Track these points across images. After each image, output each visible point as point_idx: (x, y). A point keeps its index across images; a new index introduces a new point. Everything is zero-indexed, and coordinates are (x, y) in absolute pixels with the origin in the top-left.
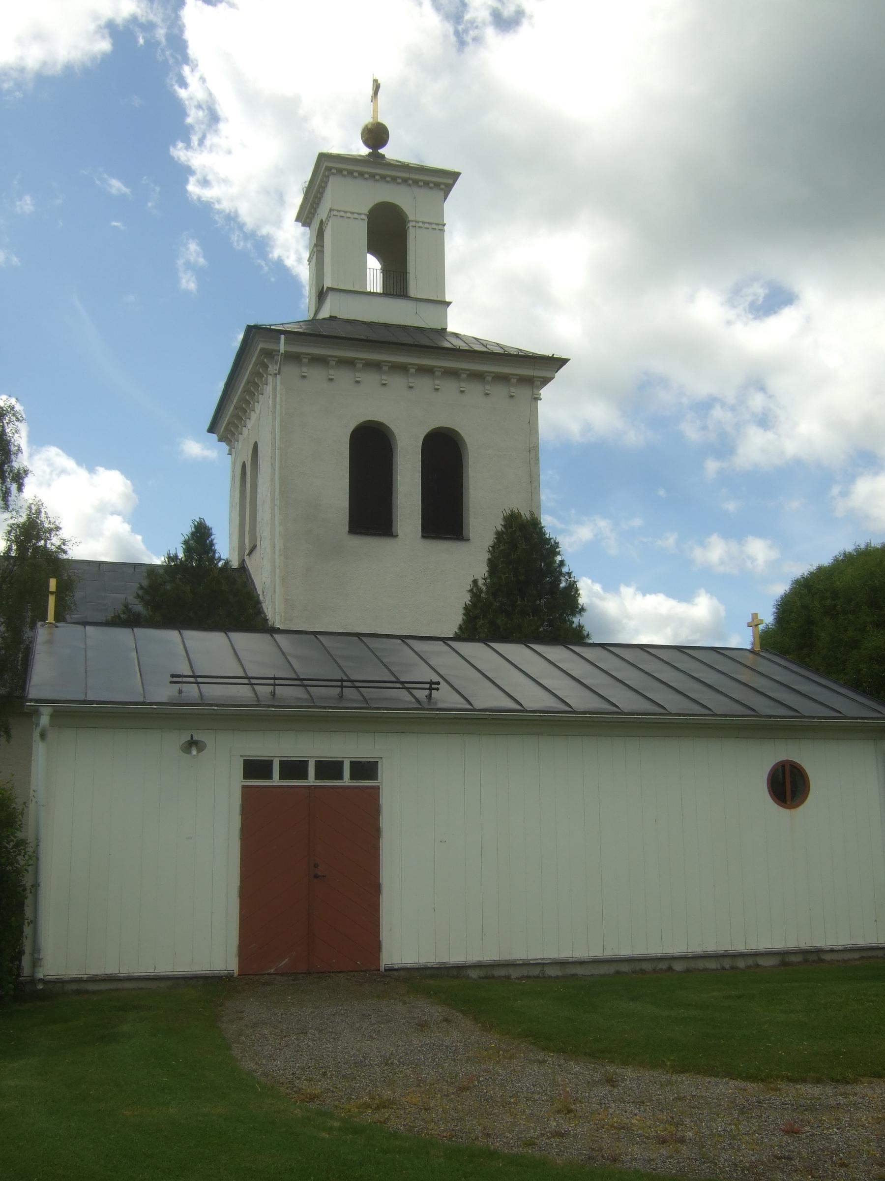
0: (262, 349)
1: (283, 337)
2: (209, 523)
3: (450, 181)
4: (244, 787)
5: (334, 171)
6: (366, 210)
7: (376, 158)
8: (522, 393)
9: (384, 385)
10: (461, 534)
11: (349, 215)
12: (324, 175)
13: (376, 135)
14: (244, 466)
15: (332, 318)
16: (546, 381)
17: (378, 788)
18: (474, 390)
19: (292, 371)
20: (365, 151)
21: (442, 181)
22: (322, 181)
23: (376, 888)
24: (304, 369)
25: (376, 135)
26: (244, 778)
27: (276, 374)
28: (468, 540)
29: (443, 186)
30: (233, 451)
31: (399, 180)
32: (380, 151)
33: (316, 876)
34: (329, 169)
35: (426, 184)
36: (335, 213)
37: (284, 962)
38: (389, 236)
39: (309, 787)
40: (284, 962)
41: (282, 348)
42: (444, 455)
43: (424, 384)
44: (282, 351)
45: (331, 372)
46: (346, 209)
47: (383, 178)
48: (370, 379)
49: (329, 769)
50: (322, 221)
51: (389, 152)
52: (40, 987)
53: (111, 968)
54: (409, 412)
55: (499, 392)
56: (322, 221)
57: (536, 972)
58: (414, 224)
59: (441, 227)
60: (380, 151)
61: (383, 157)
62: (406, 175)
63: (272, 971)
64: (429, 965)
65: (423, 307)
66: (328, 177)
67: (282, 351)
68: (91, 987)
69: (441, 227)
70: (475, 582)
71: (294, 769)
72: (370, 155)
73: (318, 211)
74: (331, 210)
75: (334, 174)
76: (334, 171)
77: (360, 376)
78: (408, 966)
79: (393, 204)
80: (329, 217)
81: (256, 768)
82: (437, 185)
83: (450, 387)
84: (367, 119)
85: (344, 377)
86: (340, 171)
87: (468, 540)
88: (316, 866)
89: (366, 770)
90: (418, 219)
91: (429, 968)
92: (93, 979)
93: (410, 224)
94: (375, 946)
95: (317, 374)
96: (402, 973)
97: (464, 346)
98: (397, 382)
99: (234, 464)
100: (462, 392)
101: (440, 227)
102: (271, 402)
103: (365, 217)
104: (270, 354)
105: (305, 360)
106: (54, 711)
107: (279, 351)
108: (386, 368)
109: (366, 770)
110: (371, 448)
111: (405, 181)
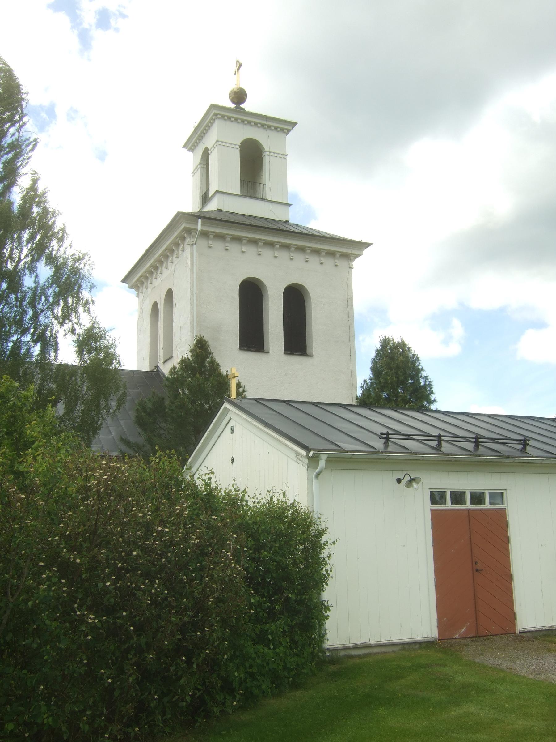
0: (185, 227)
1: (200, 220)
2: (206, 338)
3: (290, 128)
4: (432, 510)
5: (219, 116)
6: (239, 143)
7: (239, 110)
8: (342, 263)
9: (259, 254)
10: (265, 349)
11: (228, 145)
12: (212, 119)
13: (239, 96)
14: (155, 306)
15: (219, 210)
16: (357, 256)
17: (505, 510)
18: (314, 260)
19: (203, 243)
20: (232, 106)
21: (284, 127)
22: (210, 122)
23: (510, 577)
24: (210, 242)
25: (239, 96)
26: (432, 504)
27: (193, 244)
28: (312, 356)
29: (285, 131)
30: (141, 295)
31: (259, 125)
32: (242, 106)
33: (477, 570)
34: (216, 115)
35: (276, 128)
36: (220, 143)
37: (463, 630)
38: (252, 161)
39: (468, 510)
40: (463, 630)
41: (200, 227)
42: (296, 300)
43: (284, 255)
44: (199, 229)
45: (227, 245)
46: (227, 141)
47: (243, 121)
48: (251, 250)
49: (477, 498)
50: (206, 149)
51: (247, 106)
52: (328, 654)
53: (364, 639)
54: (276, 273)
55: (329, 262)
56: (206, 149)
57: (545, 633)
58: (268, 153)
59: (284, 156)
60: (242, 106)
61: (244, 109)
62: (264, 122)
63: (457, 636)
64: (544, 628)
65: (275, 206)
66: (214, 120)
67: (199, 229)
68: (354, 653)
69: (284, 156)
70: (365, 381)
71: (458, 498)
72: (235, 107)
73: (203, 141)
74: (217, 141)
75: (219, 118)
76: (219, 116)
77: (245, 248)
78: (533, 629)
79: (255, 140)
80: (214, 146)
81: (437, 497)
82: (282, 130)
83: (299, 258)
84: (232, 86)
85: (235, 248)
86: (223, 117)
87: (312, 356)
88: (476, 563)
89: (498, 496)
90: (271, 151)
91: (544, 630)
92: (356, 647)
93: (266, 154)
94: (513, 617)
95: (218, 246)
96: (529, 634)
97: (306, 232)
98: (268, 253)
99: (141, 304)
100: (307, 261)
101: (284, 156)
102: (189, 262)
103: (238, 147)
104: (189, 231)
105: (212, 236)
106: (328, 458)
107: (197, 230)
108: (261, 244)
109: (498, 496)
110: (251, 294)
111: (263, 126)
